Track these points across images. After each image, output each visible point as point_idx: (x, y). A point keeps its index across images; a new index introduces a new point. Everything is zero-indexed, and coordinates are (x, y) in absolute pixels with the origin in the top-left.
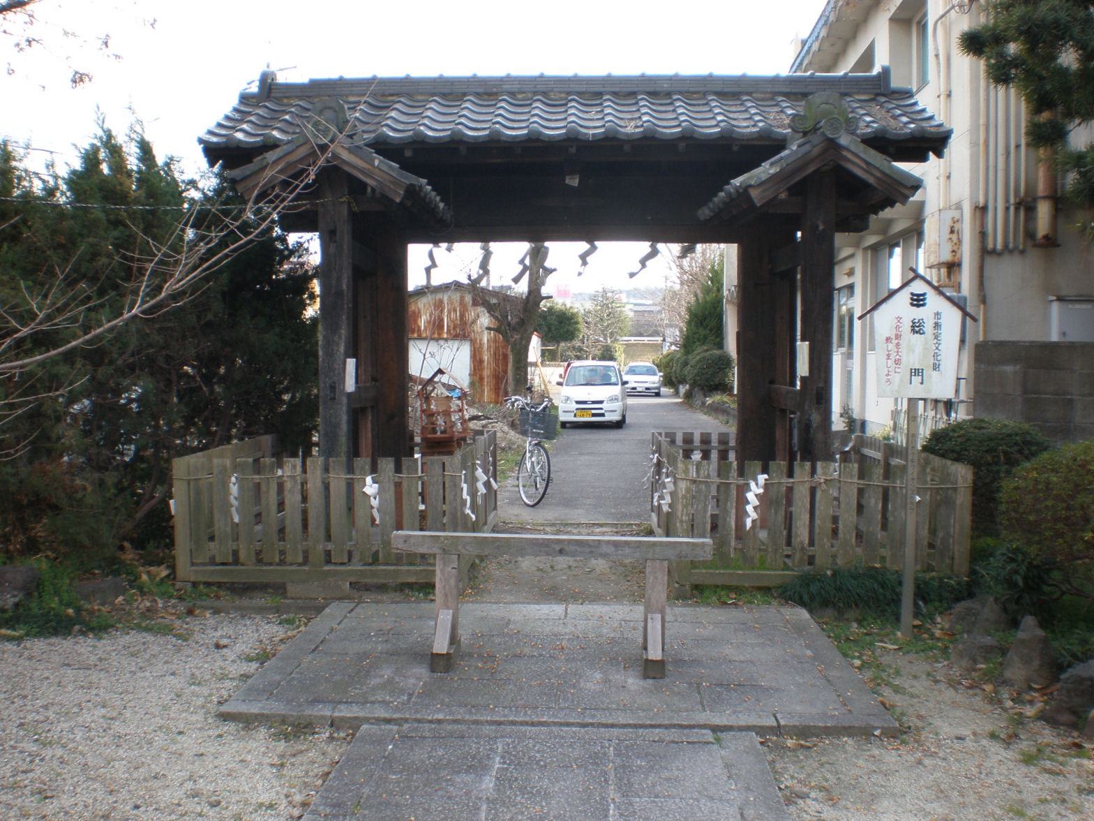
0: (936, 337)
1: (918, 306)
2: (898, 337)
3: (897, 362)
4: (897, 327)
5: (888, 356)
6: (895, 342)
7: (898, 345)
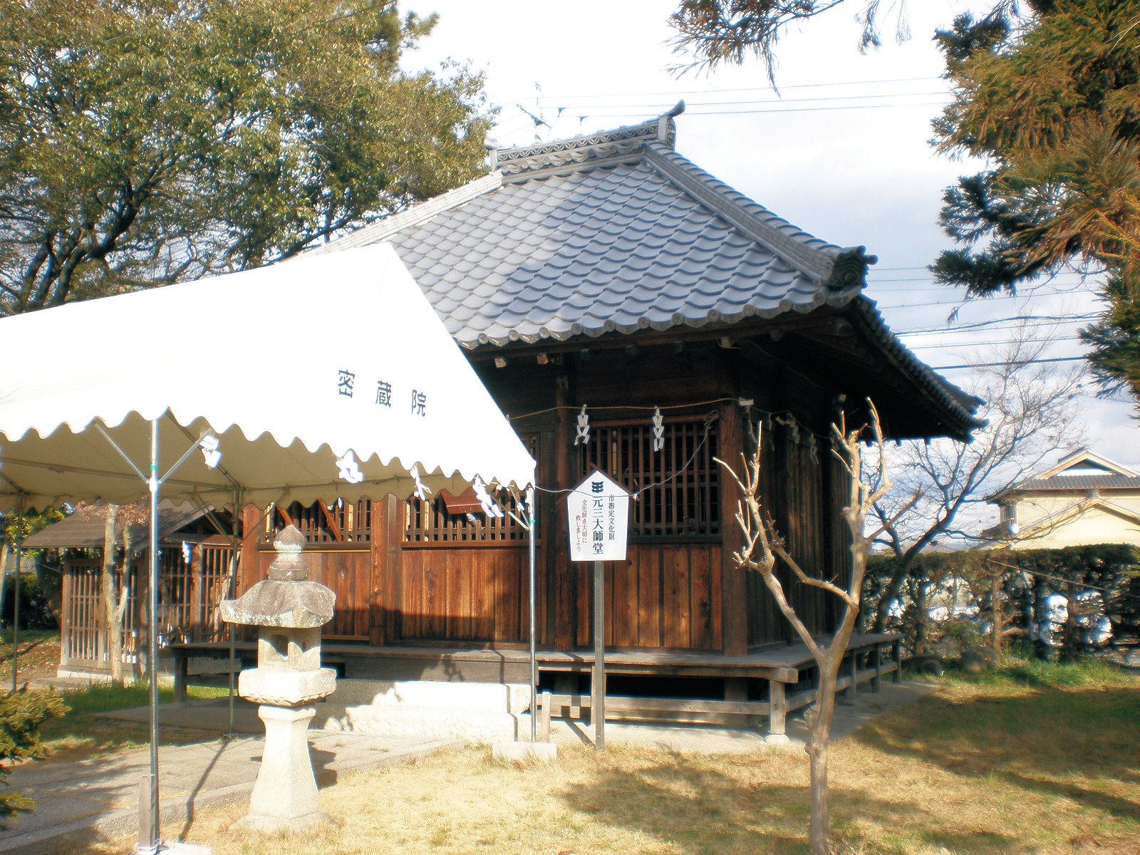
0: (611, 514)
2: (584, 515)
6: (582, 519)
7: (584, 521)
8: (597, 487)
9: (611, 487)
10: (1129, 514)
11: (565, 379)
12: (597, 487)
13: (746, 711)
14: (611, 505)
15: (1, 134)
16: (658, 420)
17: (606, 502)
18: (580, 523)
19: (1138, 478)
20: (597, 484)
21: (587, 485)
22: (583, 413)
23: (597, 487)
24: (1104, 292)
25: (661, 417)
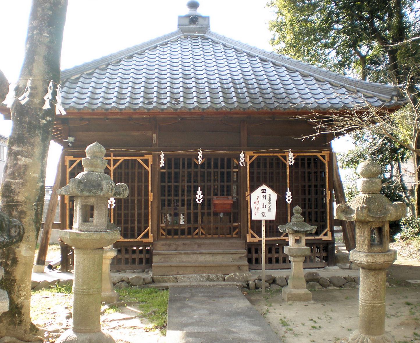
0: (269, 202)
1: (264, 193)
2: (258, 202)
3: (258, 209)
4: (258, 199)
5: (255, 207)
6: (257, 203)
7: (258, 204)
8: (264, 191)
9: (269, 191)
10: (121, 318)
11: (154, 143)
12: (264, 191)
13: (309, 260)
14: (269, 198)
15: (419, 26)
16: (162, 156)
17: (267, 197)
18: (256, 204)
19: (419, 283)
20: (264, 190)
21: (258, 191)
22: (290, 152)
23: (264, 191)
24: (89, 307)
25: (164, 155)
